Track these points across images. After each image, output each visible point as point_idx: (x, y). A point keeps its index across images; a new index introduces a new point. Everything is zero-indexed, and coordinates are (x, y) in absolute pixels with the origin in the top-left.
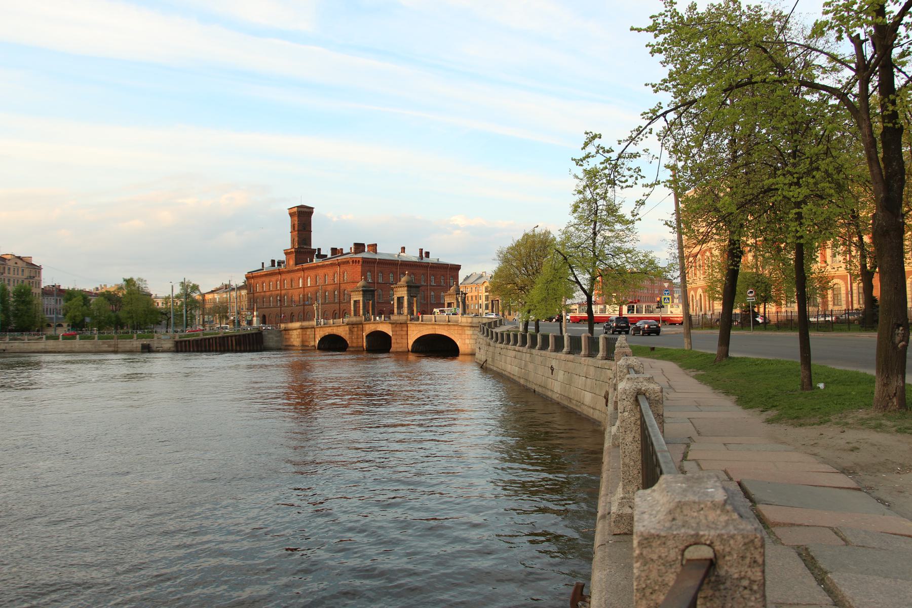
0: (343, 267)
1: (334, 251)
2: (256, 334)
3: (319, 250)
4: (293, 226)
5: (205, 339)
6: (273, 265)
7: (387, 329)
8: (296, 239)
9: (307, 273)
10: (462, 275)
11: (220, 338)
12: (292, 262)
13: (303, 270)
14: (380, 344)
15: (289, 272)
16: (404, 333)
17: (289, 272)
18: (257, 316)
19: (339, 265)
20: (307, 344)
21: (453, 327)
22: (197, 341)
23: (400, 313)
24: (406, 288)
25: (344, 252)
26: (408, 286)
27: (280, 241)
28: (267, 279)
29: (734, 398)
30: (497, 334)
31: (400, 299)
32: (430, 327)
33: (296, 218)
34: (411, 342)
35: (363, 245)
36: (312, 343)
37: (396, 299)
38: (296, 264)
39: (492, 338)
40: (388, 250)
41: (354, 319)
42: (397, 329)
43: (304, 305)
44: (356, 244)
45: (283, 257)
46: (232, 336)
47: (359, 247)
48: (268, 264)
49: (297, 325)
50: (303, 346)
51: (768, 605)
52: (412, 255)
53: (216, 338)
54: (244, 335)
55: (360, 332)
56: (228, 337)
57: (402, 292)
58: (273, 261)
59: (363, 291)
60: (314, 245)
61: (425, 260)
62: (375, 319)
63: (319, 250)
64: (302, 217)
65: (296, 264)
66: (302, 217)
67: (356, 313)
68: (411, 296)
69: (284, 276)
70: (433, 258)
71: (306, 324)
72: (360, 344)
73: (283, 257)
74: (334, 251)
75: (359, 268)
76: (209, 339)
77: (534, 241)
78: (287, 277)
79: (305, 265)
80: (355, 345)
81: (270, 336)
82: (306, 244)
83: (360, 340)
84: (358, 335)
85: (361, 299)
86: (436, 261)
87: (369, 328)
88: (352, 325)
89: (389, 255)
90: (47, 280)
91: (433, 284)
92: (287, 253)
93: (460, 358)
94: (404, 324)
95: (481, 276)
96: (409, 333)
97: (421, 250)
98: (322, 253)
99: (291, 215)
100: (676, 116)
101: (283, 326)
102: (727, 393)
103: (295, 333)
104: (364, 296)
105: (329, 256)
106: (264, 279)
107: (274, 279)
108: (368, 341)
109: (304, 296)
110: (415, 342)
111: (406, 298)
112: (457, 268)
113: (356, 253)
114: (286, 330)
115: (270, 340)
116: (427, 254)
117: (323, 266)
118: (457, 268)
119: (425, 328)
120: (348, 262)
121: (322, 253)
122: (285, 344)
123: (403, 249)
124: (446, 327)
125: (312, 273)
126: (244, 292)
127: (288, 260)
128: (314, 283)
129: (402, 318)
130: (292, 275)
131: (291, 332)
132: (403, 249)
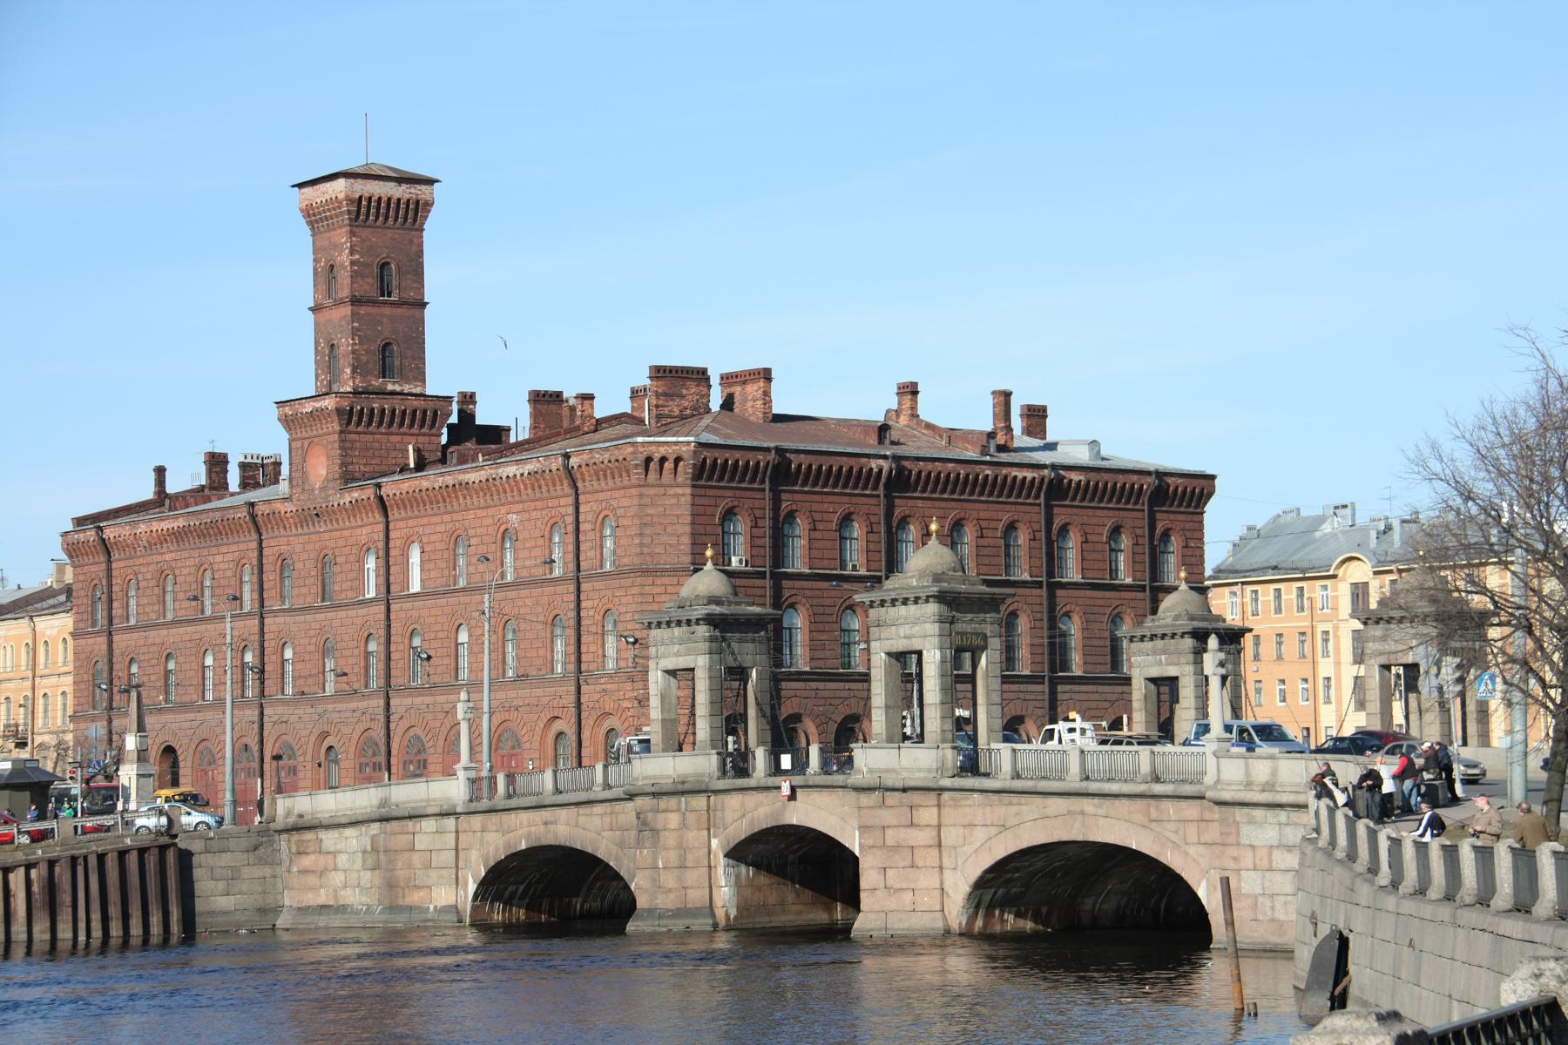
1: (545, 402)
3: (468, 399)
4: (326, 274)
8: (345, 344)
12: (321, 468)
16: (923, 837)
18: (142, 755)
24: (937, 639)
31: (906, 663)
33: (342, 237)
34: (959, 885)
37: (879, 660)
38: (348, 478)
42: (888, 817)
44: (659, 373)
45: (273, 442)
47: (676, 383)
51: (17, 628)
55: (695, 837)
57: (908, 627)
58: (217, 462)
60: (442, 377)
63: (468, 399)
68: (962, 652)
71: (406, 793)
72: (697, 897)
73: (273, 442)
74: (545, 402)
75: (677, 498)
77: (1518, 438)
80: (667, 902)
83: (694, 877)
84: (683, 849)
85: (701, 663)
86: (1082, 456)
92: (293, 417)
96: (950, 836)
99: (314, 217)
100: (1489, 569)
104: (718, 646)
105: (521, 430)
110: (981, 884)
113: (664, 423)
116: (1036, 417)
126: (56, 626)
130: (324, 536)
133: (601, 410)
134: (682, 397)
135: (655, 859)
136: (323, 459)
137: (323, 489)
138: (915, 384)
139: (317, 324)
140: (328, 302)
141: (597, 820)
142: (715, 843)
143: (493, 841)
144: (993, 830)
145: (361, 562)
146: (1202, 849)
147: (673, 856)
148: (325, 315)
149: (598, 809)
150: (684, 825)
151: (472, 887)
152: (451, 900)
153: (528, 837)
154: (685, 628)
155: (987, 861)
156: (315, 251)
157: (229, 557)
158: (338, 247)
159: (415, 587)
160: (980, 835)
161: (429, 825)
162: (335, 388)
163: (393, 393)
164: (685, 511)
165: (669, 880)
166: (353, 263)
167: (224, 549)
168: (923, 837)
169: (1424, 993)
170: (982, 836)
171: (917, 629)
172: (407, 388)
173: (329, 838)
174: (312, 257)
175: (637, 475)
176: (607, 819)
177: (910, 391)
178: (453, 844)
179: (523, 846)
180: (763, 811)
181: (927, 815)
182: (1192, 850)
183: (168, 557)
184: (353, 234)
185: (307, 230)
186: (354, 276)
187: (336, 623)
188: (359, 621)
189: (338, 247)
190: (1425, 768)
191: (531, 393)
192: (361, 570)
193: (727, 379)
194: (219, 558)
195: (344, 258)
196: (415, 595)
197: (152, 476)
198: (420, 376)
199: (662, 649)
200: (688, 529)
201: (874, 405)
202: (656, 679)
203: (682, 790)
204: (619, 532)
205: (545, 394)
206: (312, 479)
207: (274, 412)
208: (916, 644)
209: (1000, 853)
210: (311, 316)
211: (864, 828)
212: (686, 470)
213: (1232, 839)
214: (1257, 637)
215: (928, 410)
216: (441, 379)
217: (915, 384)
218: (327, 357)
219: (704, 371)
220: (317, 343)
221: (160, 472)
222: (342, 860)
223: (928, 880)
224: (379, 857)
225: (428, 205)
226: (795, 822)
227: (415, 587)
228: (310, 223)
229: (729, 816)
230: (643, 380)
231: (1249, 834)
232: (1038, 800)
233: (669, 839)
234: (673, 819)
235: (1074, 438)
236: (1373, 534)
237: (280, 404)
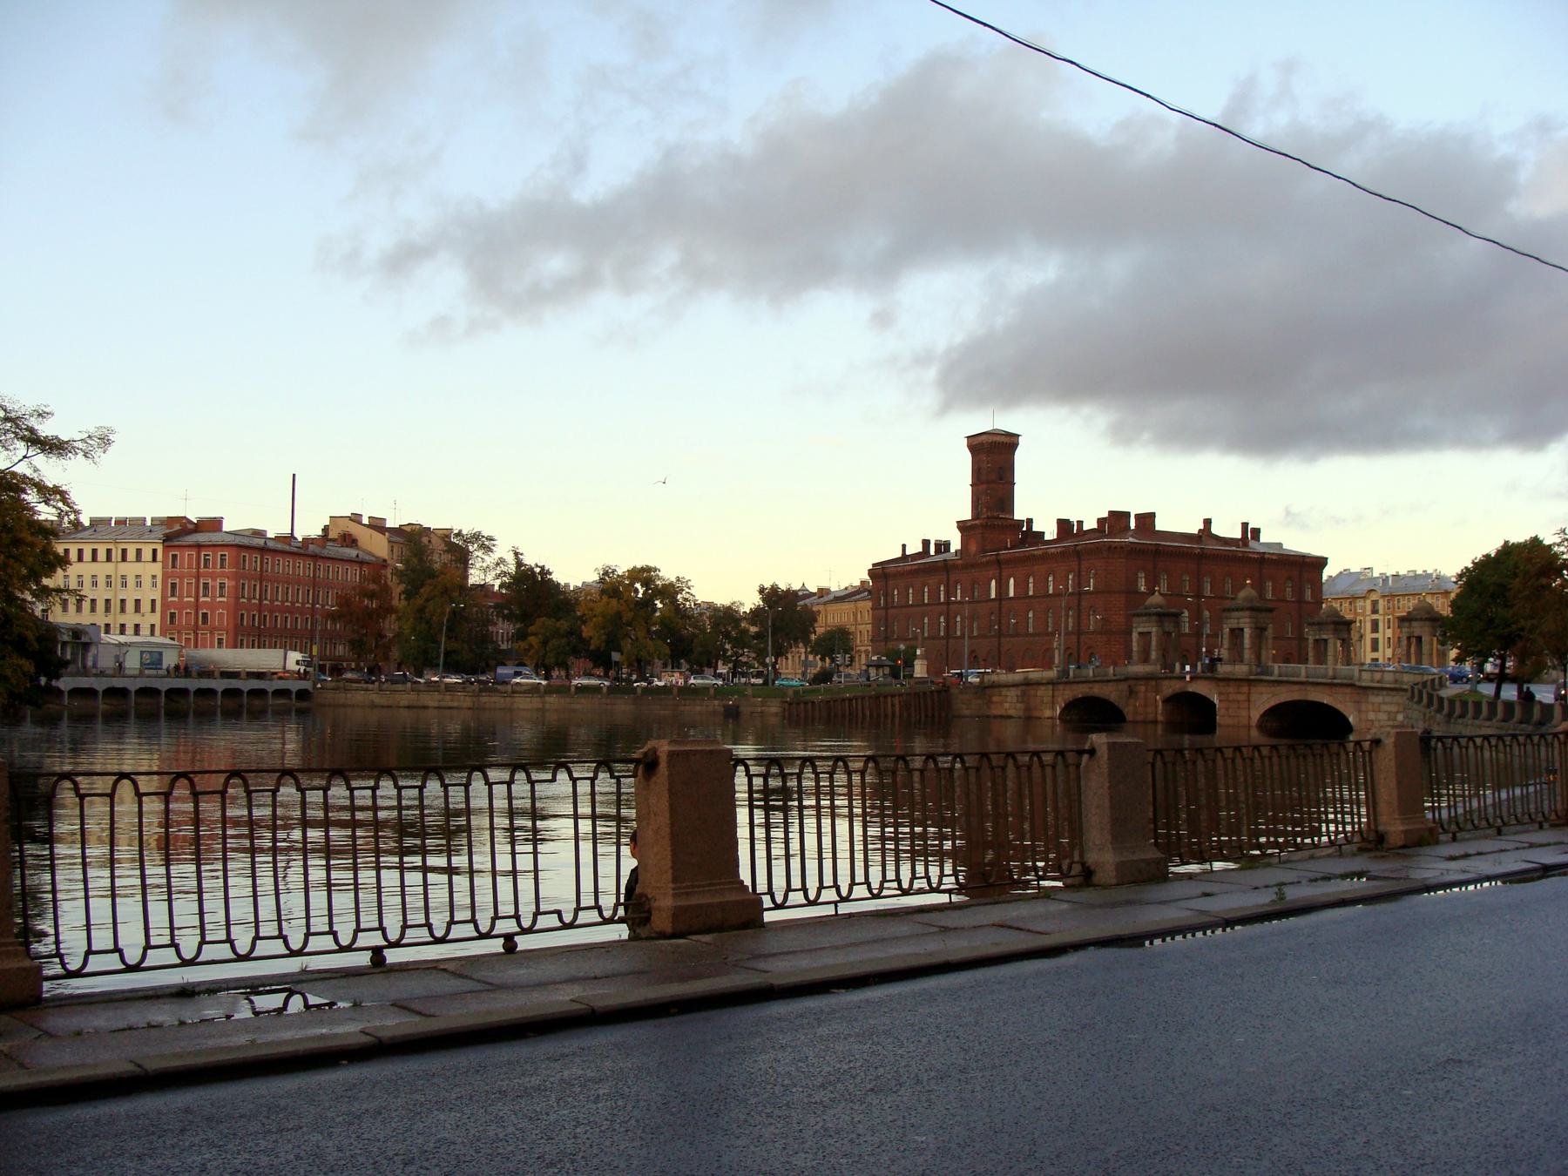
2: (939, 692)
3: (1030, 521)
10: (1327, 573)
29: (482, 573)
30: (1441, 699)
34: (1256, 715)
39: (1440, 710)
42: (1231, 689)
43: (1000, 634)
58: (926, 543)
60: (1020, 514)
63: (1030, 521)
68: (1259, 631)
82: (1003, 511)
90: (271, 535)
92: (962, 526)
96: (1253, 697)
97: (1245, 525)
102: (121, 522)
111: (1247, 632)
112: (1321, 562)
116: (1256, 532)
118: (1321, 562)
129: (1241, 670)
133: (1086, 527)
143: (1067, 694)
155: (1267, 707)
159: (1012, 594)
160: (1265, 697)
165: (1140, 710)
168: (1242, 697)
170: (1264, 700)
173: (1004, 691)
177: (1208, 522)
181: (1245, 689)
190: (833, 660)
201: (1194, 527)
202: (1135, 636)
203: (1147, 678)
211: (1220, 694)
215: (1215, 530)
223: (1244, 713)
224: (1024, 697)
227: (1012, 594)
233: (1141, 695)
234: (1143, 688)
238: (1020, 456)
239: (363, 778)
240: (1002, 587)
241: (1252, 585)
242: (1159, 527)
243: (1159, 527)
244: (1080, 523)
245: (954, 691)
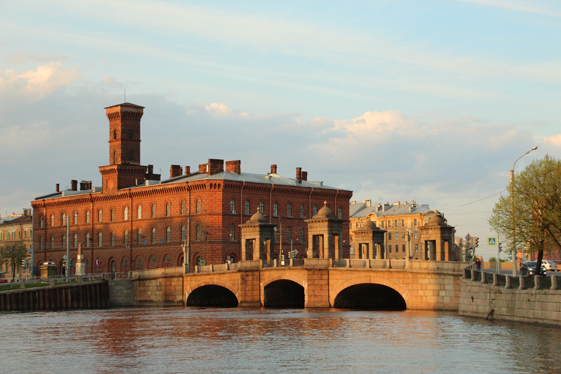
0: (195, 194)
1: (176, 170)
2: (100, 284)
3: (151, 167)
4: (114, 134)
5: (29, 292)
6: (74, 188)
7: (298, 277)
8: (119, 151)
9: (136, 200)
11: (49, 290)
12: (112, 184)
13: (131, 196)
14: (286, 295)
15: (107, 198)
16: (324, 282)
17: (107, 198)
19: (189, 189)
20: (171, 298)
21: (396, 275)
22: (17, 294)
23: (317, 256)
24: (326, 224)
25: (192, 171)
26: (329, 221)
27: (92, 155)
28: (70, 209)
31: (249, 243)
32: (363, 274)
33: (118, 122)
34: (333, 296)
35: (221, 162)
36: (179, 298)
38: (120, 187)
40: (254, 169)
41: (248, 264)
42: (315, 277)
45: (97, 181)
46: (66, 288)
47: (216, 165)
48: (65, 186)
49: (159, 272)
50: (166, 301)
52: (286, 176)
53: (44, 291)
54: (84, 287)
55: (256, 282)
56: (61, 289)
58: (74, 183)
59: (260, 226)
60: (144, 162)
61: (304, 184)
62: (278, 264)
63: (151, 167)
64: (128, 121)
65: (120, 187)
66: (128, 121)
67: (250, 256)
69: (98, 205)
70: (313, 181)
71: (171, 271)
72: (256, 298)
74: (176, 170)
75: (219, 195)
76: (34, 292)
78: (106, 206)
79: (134, 190)
80: (249, 299)
81: (118, 288)
82: (132, 159)
83: (256, 293)
84: (253, 285)
85: (258, 237)
86: (318, 185)
87: (270, 276)
88: (245, 272)
89: (255, 176)
91: (275, 214)
93: (407, 311)
94: (325, 270)
95: (364, 207)
98: (155, 172)
99: (111, 117)
101: (136, 274)
103: (154, 283)
104: (261, 233)
106: (64, 208)
107: (81, 208)
108: (266, 295)
109: (131, 232)
111: (326, 236)
112: (348, 195)
114: (141, 280)
115: (119, 292)
117: (155, 192)
118: (348, 195)
119: (355, 275)
120: (204, 186)
121: (155, 172)
122: (139, 298)
123: (274, 168)
124: (386, 275)
125: (146, 201)
126: (28, 227)
127: (105, 182)
128: (147, 215)
129: (322, 262)
131: (147, 283)
132: (274, 168)
134: (217, 167)
135: (245, 288)
136: (112, 182)
137: (112, 190)
138: (276, 166)
139: (110, 146)
140: (114, 140)
141: (226, 278)
142: (261, 284)
144: (344, 281)
145: (124, 210)
146: (404, 285)
147: (250, 287)
148: (113, 143)
149: (226, 275)
150: (253, 279)
151: (187, 296)
152: (181, 299)
153: (204, 282)
154: (253, 228)
155: (342, 289)
156: (110, 126)
157: (83, 209)
158: (118, 125)
160: (340, 282)
161: (175, 279)
162: (116, 163)
163: (132, 165)
164: (221, 197)
166: (122, 129)
167: (81, 206)
169: (536, 311)
171: (322, 229)
172: (135, 164)
174: (109, 127)
175: (208, 188)
176: (229, 278)
178: (182, 284)
179: (203, 285)
180: (276, 276)
182: (401, 285)
183: (63, 208)
184: (122, 121)
185: (108, 120)
186: (122, 133)
187: (115, 227)
188: (123, 226)
189: (118, 125)
191: (152, 166)
192: (124, 213)
193: (228, 163)
194: (79, 209)
195: (119, 128)
196: (140, 220)
197: (56, 186)
198: (139, 160)
199: (246, 234)
200: (221, 203)
204: (202, 203)
205: (176, 166)
206: (109, 187)
207: (98, 169)
208: (322, 233)
209: (346, 286)
210: (109, 144)
212: (222, 187)
213: (415, 282)
214: (390, 234)
216: (144, 162)
217: (276, 166)
218: (113, 154)
219: (223, 161)
220: (110, 151)
221: (58, 185)
222: (151, 288)
223: (325, 293)
225: (142, 114)
226: (285, 278)
227: (140, 218)
228: (109, 118)
229: (266, 277)
230: (206, 162)
231: (421, 281)
232: (357, 273)
233: (249, 283)
235: (313, 180)
236: (377, 208)
237: (100, 167)
238: (143, 122)
239: (319, 242)
240: (133, 212)
241: (327, 205)
242: (101, 186)
243: (101, 186)
244: (188, 168)
245: (111, 284)
